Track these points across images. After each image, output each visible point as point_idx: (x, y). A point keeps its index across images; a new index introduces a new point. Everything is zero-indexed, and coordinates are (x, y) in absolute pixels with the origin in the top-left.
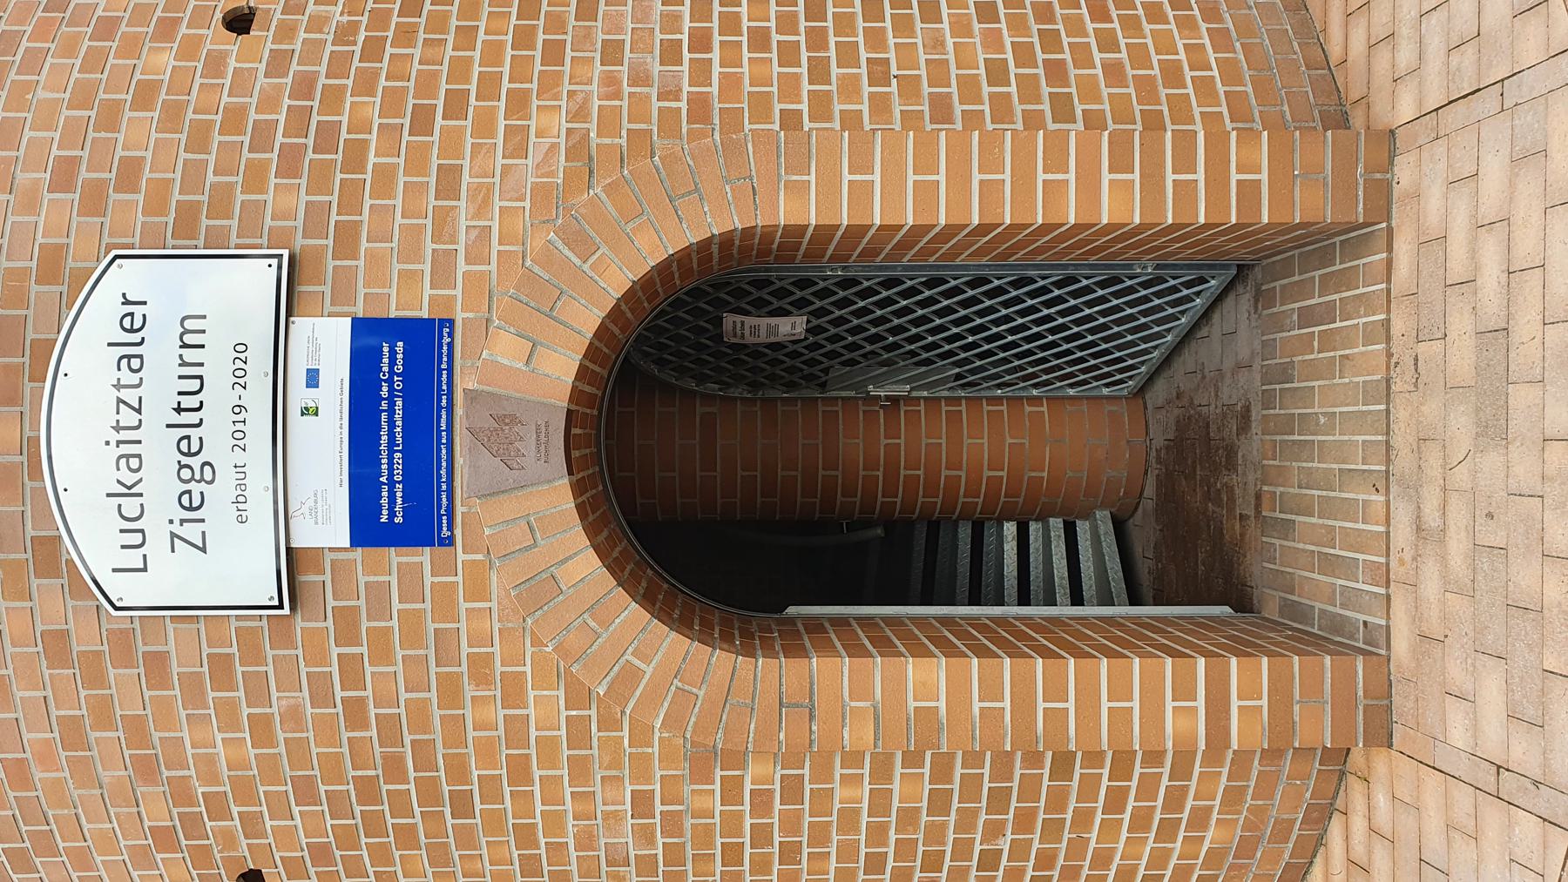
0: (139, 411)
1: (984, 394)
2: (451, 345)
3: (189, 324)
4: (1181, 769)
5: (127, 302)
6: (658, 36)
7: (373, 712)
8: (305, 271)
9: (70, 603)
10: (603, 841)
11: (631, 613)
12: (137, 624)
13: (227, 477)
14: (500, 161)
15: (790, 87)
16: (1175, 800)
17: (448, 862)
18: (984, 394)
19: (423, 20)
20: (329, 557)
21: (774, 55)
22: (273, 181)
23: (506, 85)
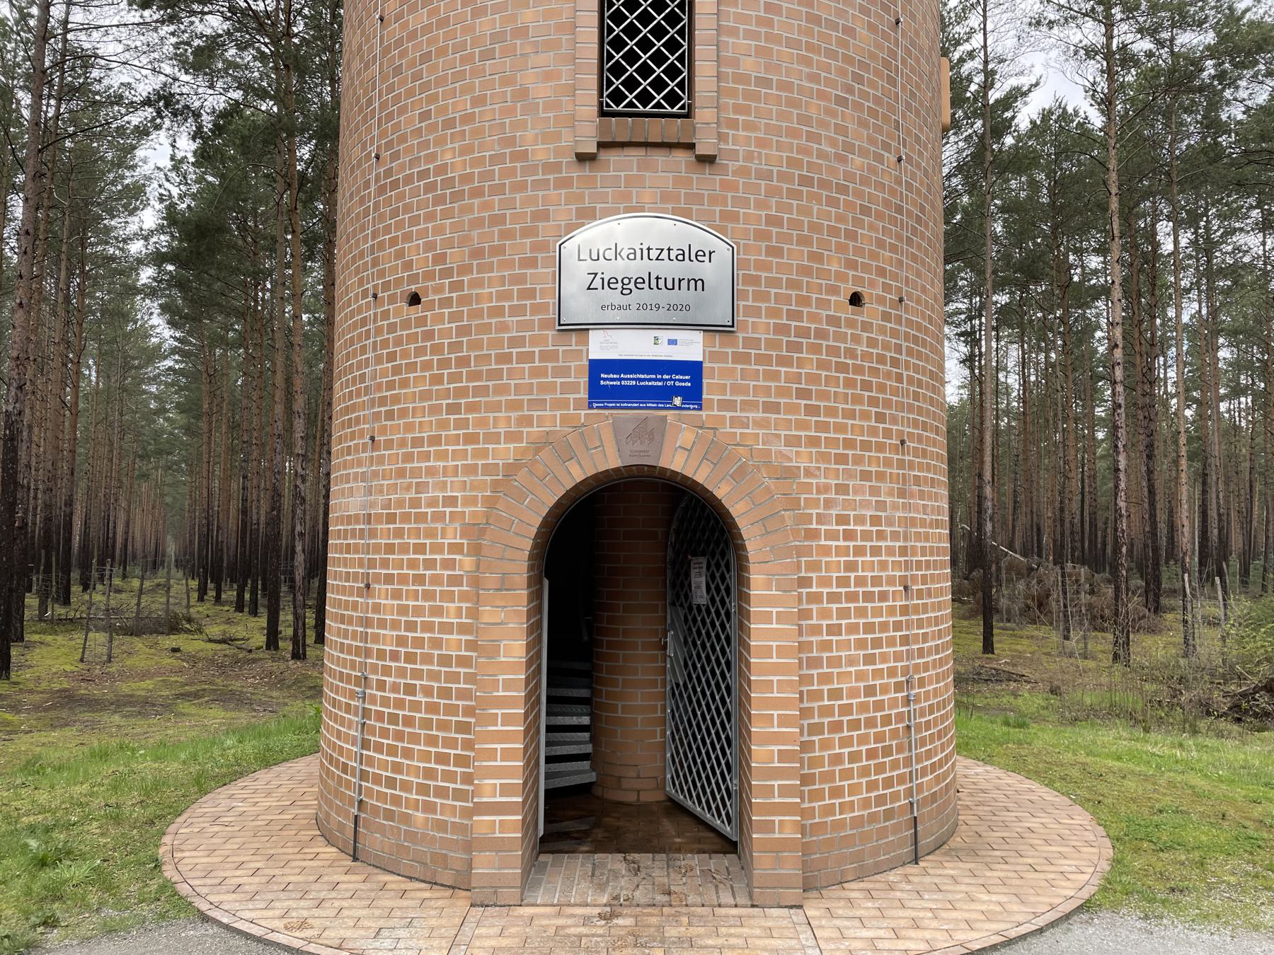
0: (657, 259)
1: (668, 702)
2: (689, 409)
3: (699, 283)
4: (460, 795)
5: (710, 253)
6: (852, 513)
7: (505, 367)
8: (726, 337)
9: (563, 223)
10: (430, 480)
11: (550, 497)
12: (552, 254)
13: (624, 300)
14: (782, 433)
15: (825, 582)
16: (441, 792)
17: (421, 399)
18: (668, 702)
19: (859, 392)
20: (584, 348)
21: (842, 574)
22: (772, 321)
23: (823, 435)
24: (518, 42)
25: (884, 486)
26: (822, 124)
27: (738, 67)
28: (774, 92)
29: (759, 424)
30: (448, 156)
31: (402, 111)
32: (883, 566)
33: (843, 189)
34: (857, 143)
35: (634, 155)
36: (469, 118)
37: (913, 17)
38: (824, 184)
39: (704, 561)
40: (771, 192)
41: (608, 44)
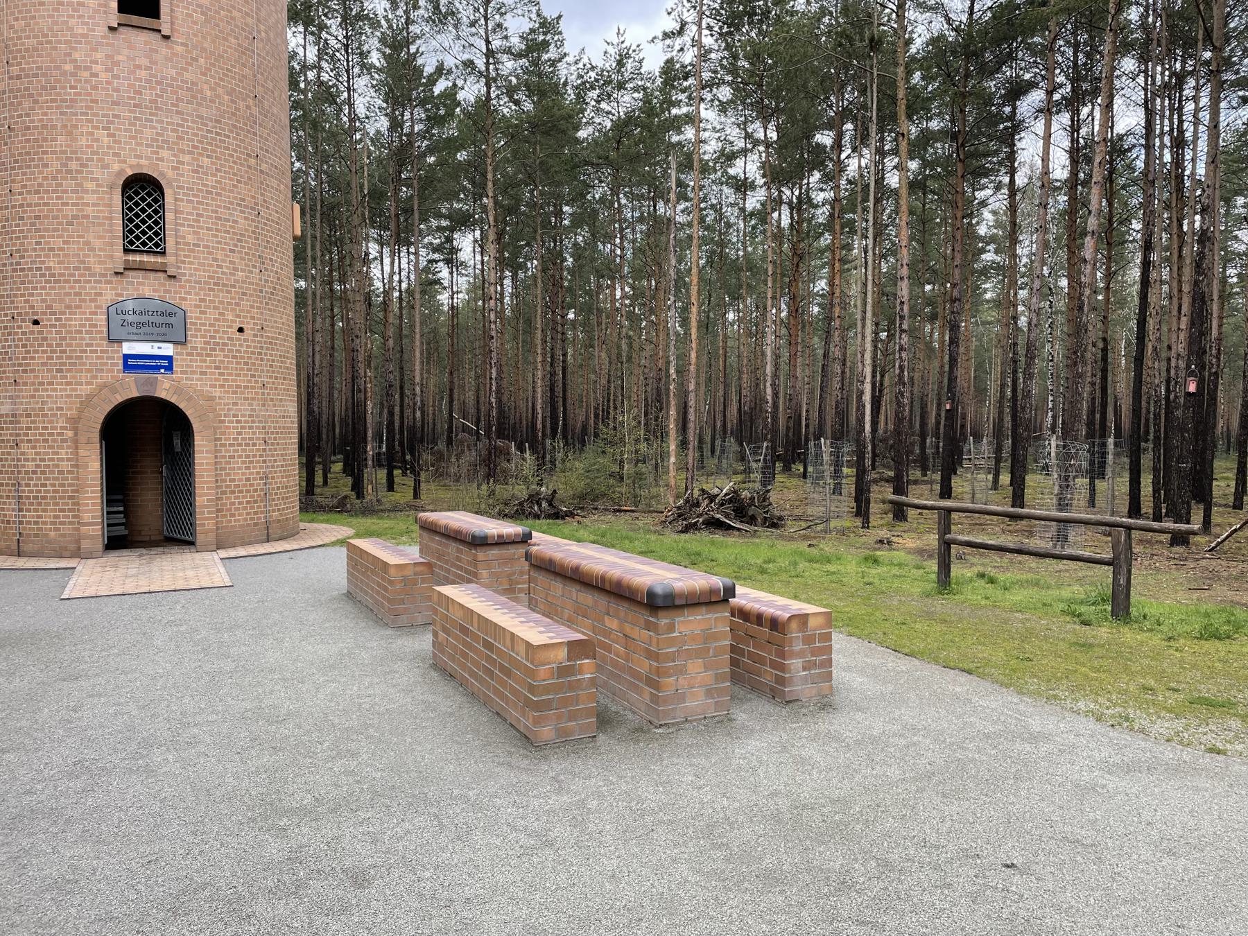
11: (109, 408)
25: (255, 403)
29: (197, 379)
32: (254, 433)
33: (233, 286)
35: (141, 274)
36: (61, 249)
39: (179, 433)
40: (201, 289)
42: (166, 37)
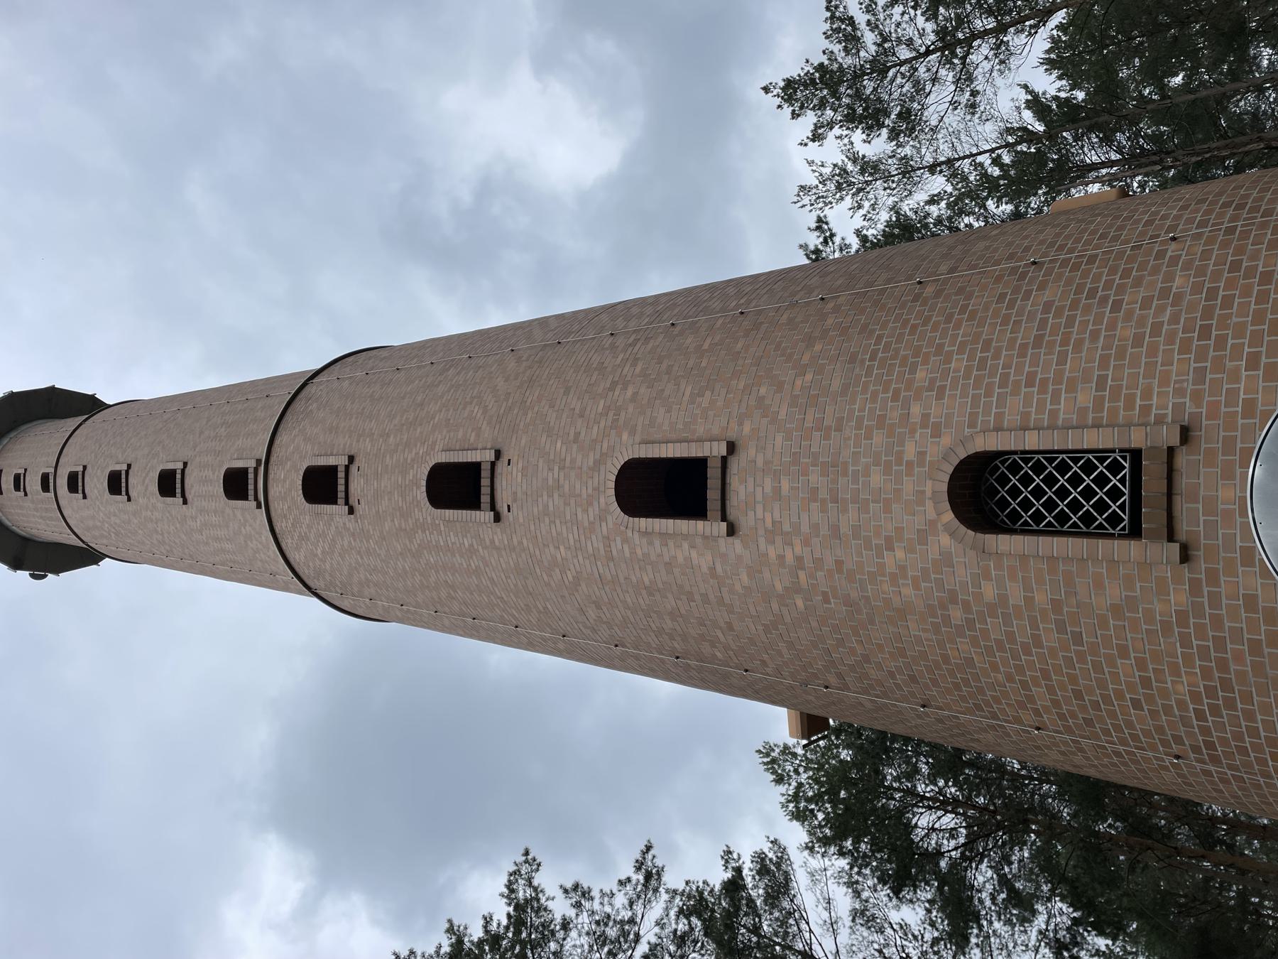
9: (1259, 581)
24: (1065, 609)
26: (1141, 322)
27: (1087, 408)
28: (1110, 373)
30: (1180, 688)
31: (1130, 725)
33: (1212, 294)
34: (1160, 285)
36: (1141, 665)
37: (1027, 249)
38: (1208, 313)
41: (1063, 527)
42: (732, 447)
